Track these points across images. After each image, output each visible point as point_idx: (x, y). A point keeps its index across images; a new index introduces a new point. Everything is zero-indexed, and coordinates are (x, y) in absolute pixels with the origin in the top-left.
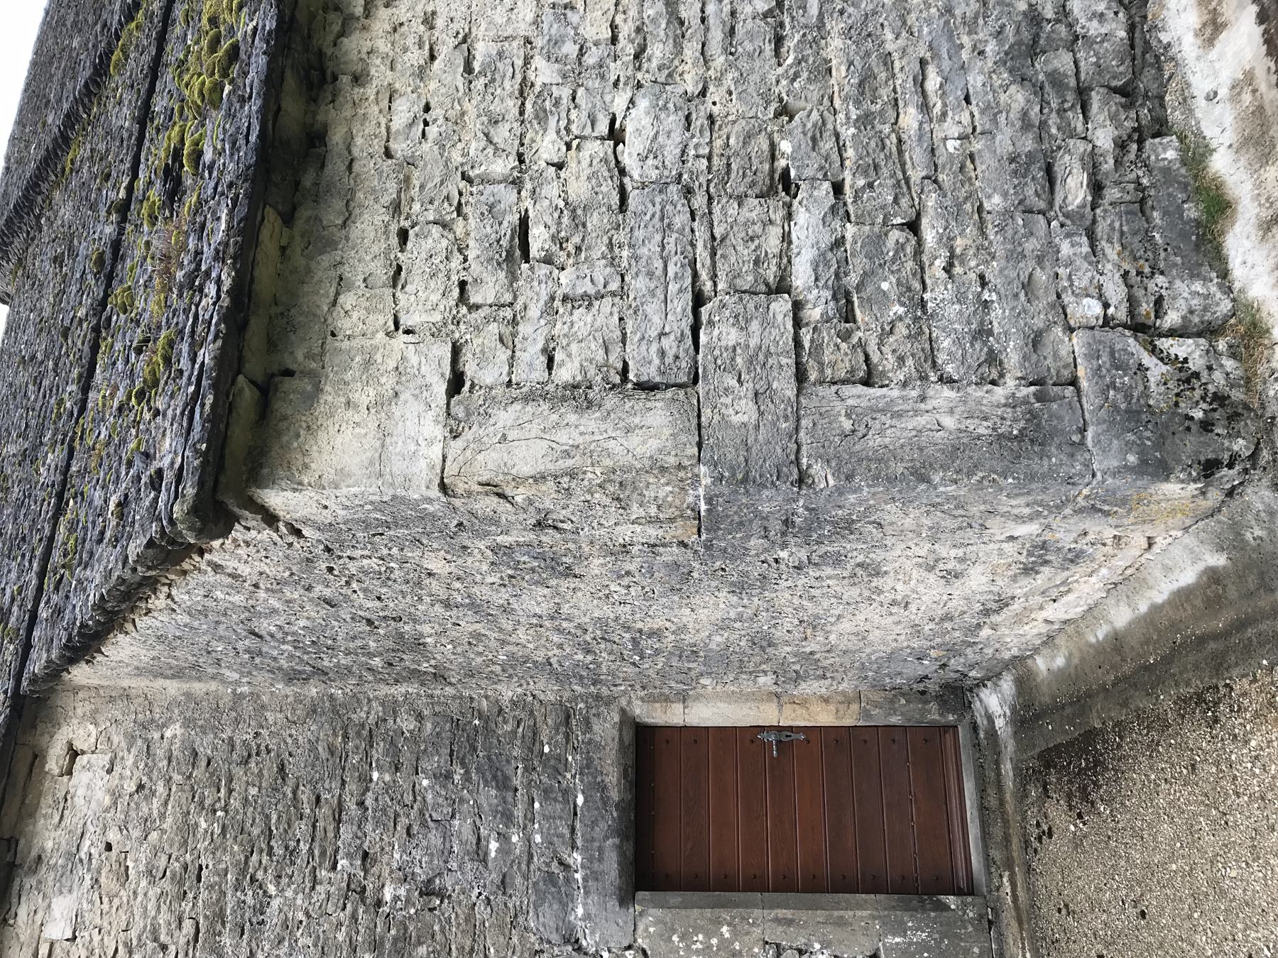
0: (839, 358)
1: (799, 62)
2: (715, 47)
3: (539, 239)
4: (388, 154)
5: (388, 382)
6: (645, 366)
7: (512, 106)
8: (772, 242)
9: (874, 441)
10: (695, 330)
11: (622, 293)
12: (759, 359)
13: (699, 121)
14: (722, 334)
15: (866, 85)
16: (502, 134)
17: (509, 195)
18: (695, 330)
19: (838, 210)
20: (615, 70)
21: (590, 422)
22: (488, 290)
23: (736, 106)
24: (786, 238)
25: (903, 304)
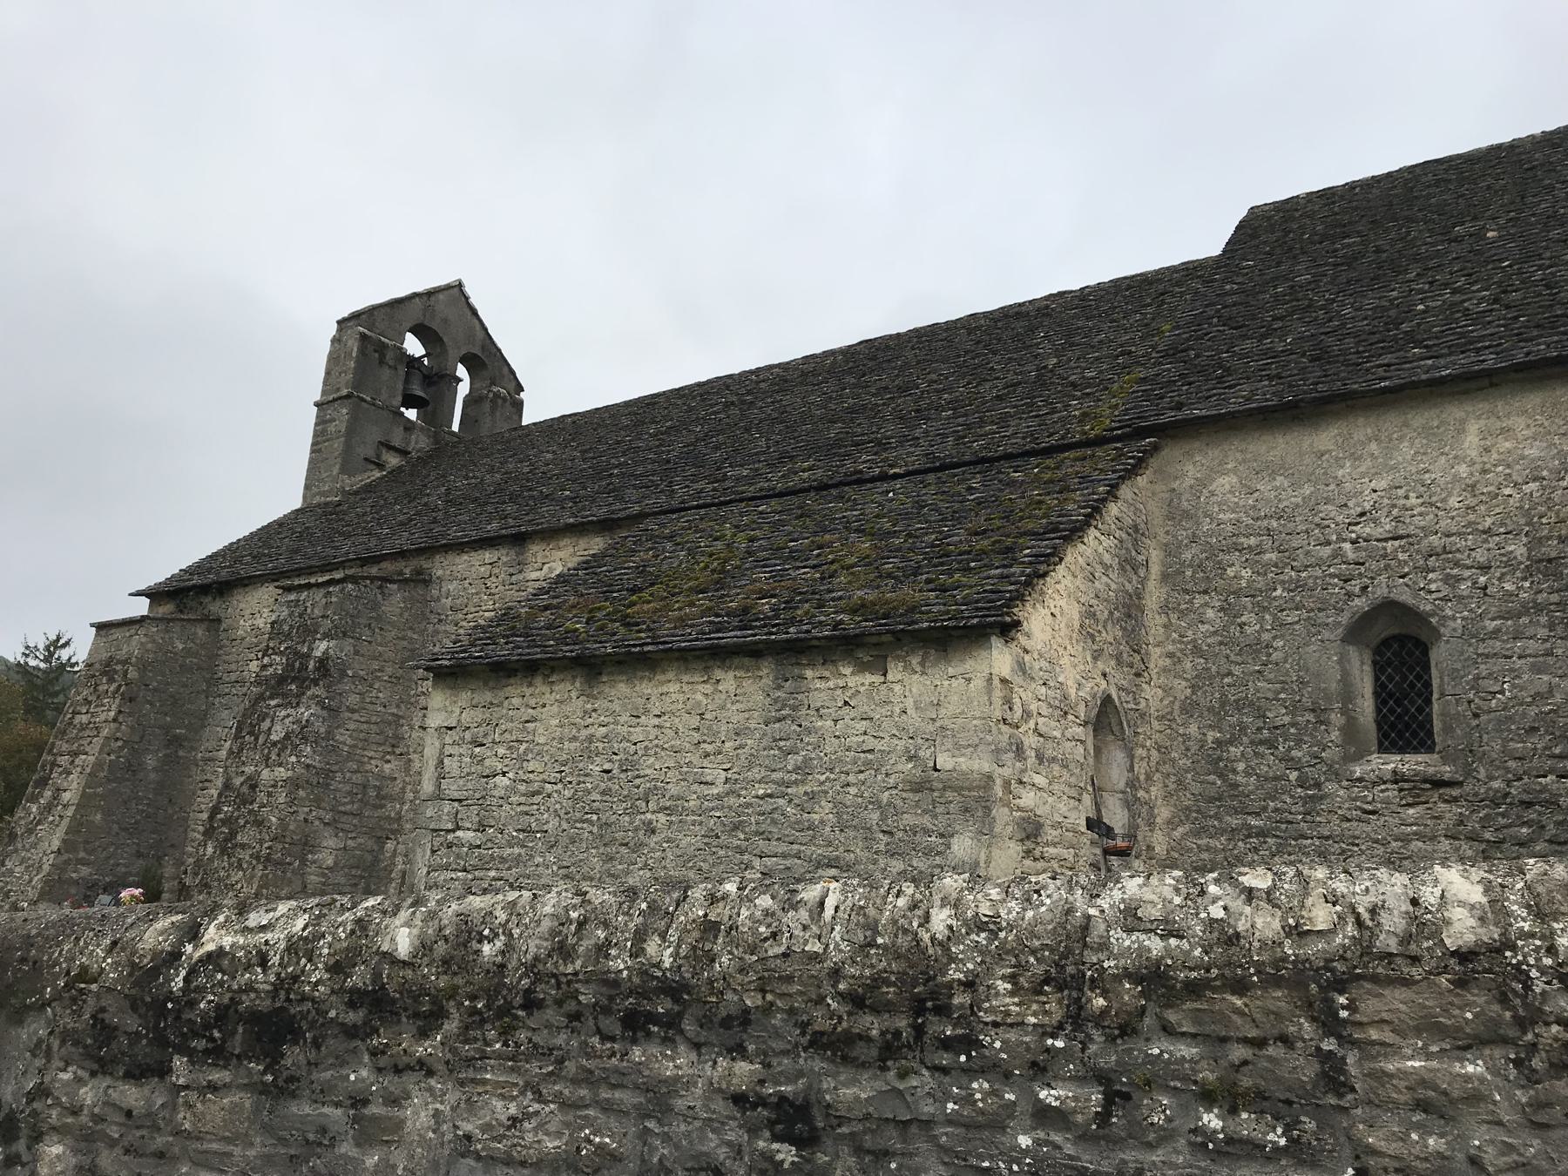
3: (478, 750)
15: (503, 860)
16: (507, 735)
19: (472, 847)
22: (468, 735)
25: (883, 1033)
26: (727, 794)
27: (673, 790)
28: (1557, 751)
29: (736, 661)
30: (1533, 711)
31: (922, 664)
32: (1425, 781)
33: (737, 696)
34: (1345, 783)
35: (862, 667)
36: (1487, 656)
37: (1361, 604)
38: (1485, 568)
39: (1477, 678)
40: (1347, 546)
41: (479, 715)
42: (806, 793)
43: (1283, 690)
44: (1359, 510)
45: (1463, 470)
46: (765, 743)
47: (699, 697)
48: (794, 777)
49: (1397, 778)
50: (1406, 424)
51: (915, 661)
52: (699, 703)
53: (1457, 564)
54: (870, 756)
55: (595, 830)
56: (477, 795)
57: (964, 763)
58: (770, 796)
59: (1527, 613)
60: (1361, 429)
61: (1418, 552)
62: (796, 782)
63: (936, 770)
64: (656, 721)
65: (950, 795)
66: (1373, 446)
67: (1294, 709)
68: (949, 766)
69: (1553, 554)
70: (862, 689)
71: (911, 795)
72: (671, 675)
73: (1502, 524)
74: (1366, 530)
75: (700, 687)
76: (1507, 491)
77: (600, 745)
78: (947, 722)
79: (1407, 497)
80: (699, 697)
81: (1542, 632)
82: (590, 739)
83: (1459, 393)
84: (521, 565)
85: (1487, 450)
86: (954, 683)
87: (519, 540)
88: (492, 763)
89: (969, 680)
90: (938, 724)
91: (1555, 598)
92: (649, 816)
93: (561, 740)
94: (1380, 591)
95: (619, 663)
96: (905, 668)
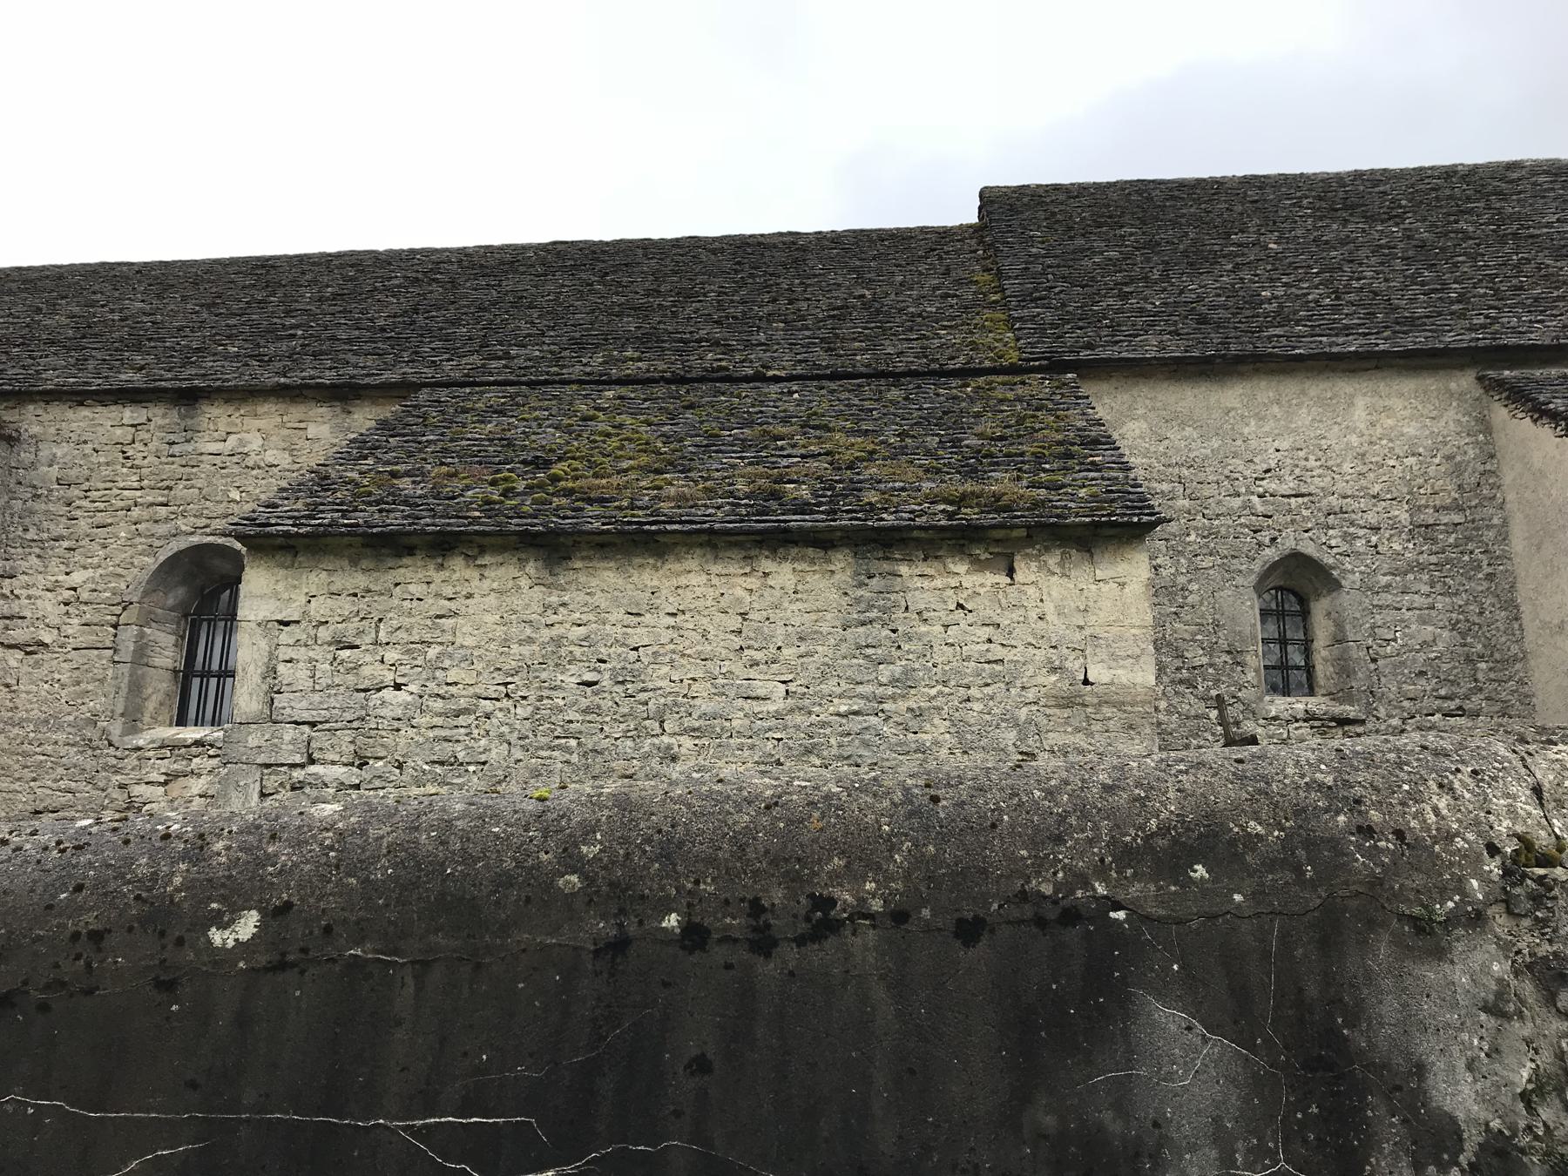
0: (271, 783)
1: (424, 771)
2: (437, 732)
3: (345, 654)
4: (397, 585)
5: (286, 596)
6: (280, 701)
7: (416, 638)
8: (331, 756)
9: (234, 794)
10: (296, 723)
11: (314, 690)
12: (276, 748)
13: (396, 724)
14: (289, 733)
16: (401, 635)
17: (368, 639)
18: (296, 723)
19: (342, 786)
20: (431, 685)
21: (257, 679)
22: (324, 634)
23: (402, 741)
24: (333, 763)
26: (792, 711)
27: (704, 706)
28: (1443, 692)
29: (794, 551)
30: (1421, 657)
31: (1061, 564)
32: (1333, 719)
33: (800, 598)
34: (1262, 722)
35: (979, 565)
36: (1381, 607)
37: (1271, 554)
38: (1376, 529)
39: (1373, 628)
40: (1255, 499)
41: (346, 605)
42: (910, 710)
43: (1200, 632)
44: (1265, 467)
45: (1354, 440)
46: (844, 649)
47: (739, 592)
48: (890, 690)
49: (1309, 717)
50: (1303, 392)
51: (1053, 560)
52: (739, 601)
53: (1352, 524)
54: (998, 668)
55: (575, 758)
56: (348, 716)
57: (1123, 676)
58: (856, 713)
59: (1411, 570)
60: (1264, 391)
61: (1319, 510)
62: (893, 698)
63: (1086, 682)
64: (671, 621)
65: (1107, 711)
66: (1275, 409)
67: (1211, 650)
68: (1106, 680)
69: (1431, 521)
70: (982, 591)
71: (1057, 711)
72: (691, 563)
73: (1389, 491)
74: (1270, 485)
75: (740, 580)
76: (1392, 463)
77: (577, 651)
78: (1098, 631)
79: (1307, 459)
80: (739, 592)
81: (1425, 589)
82: (557, 642)
83: (1344, 371)
84: (190, 433)
85: (1373, 424)
86: (1105, 588)
87: (188, 398)
88: (372, 672)
89: (1122, 585)
90: (1087, 632)
91: (1434, 559)
92: (666, 739)
93: (506, 643)
94: (1288, 542)
95: (602, 546)
96: (1039, 568)
